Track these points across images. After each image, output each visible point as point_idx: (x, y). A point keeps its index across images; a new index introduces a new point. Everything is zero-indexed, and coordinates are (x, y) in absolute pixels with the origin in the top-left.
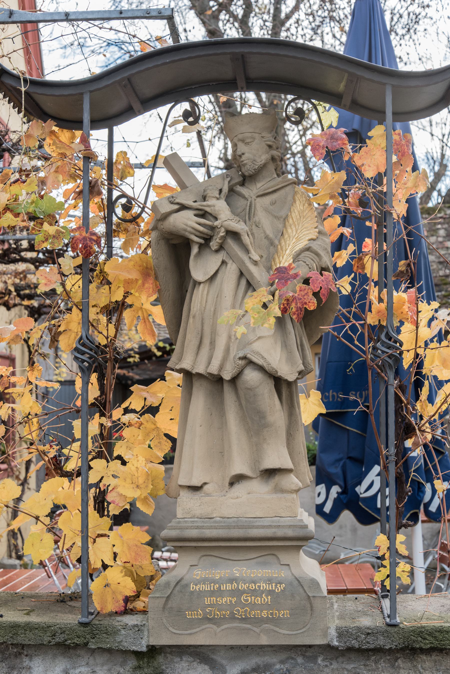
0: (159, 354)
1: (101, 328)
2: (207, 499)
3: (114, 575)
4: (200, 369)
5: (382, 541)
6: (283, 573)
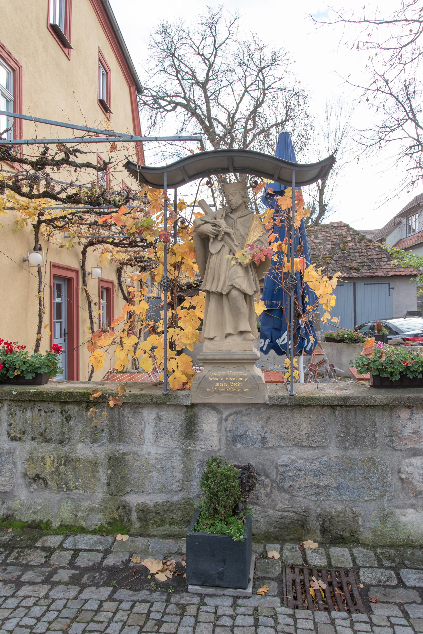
0: (195, 286)
1: (173, 273)
2: (216, 343)
3: (178, 374)
4: (213, 290)
5: (287, 361)
6: (247, 374)
